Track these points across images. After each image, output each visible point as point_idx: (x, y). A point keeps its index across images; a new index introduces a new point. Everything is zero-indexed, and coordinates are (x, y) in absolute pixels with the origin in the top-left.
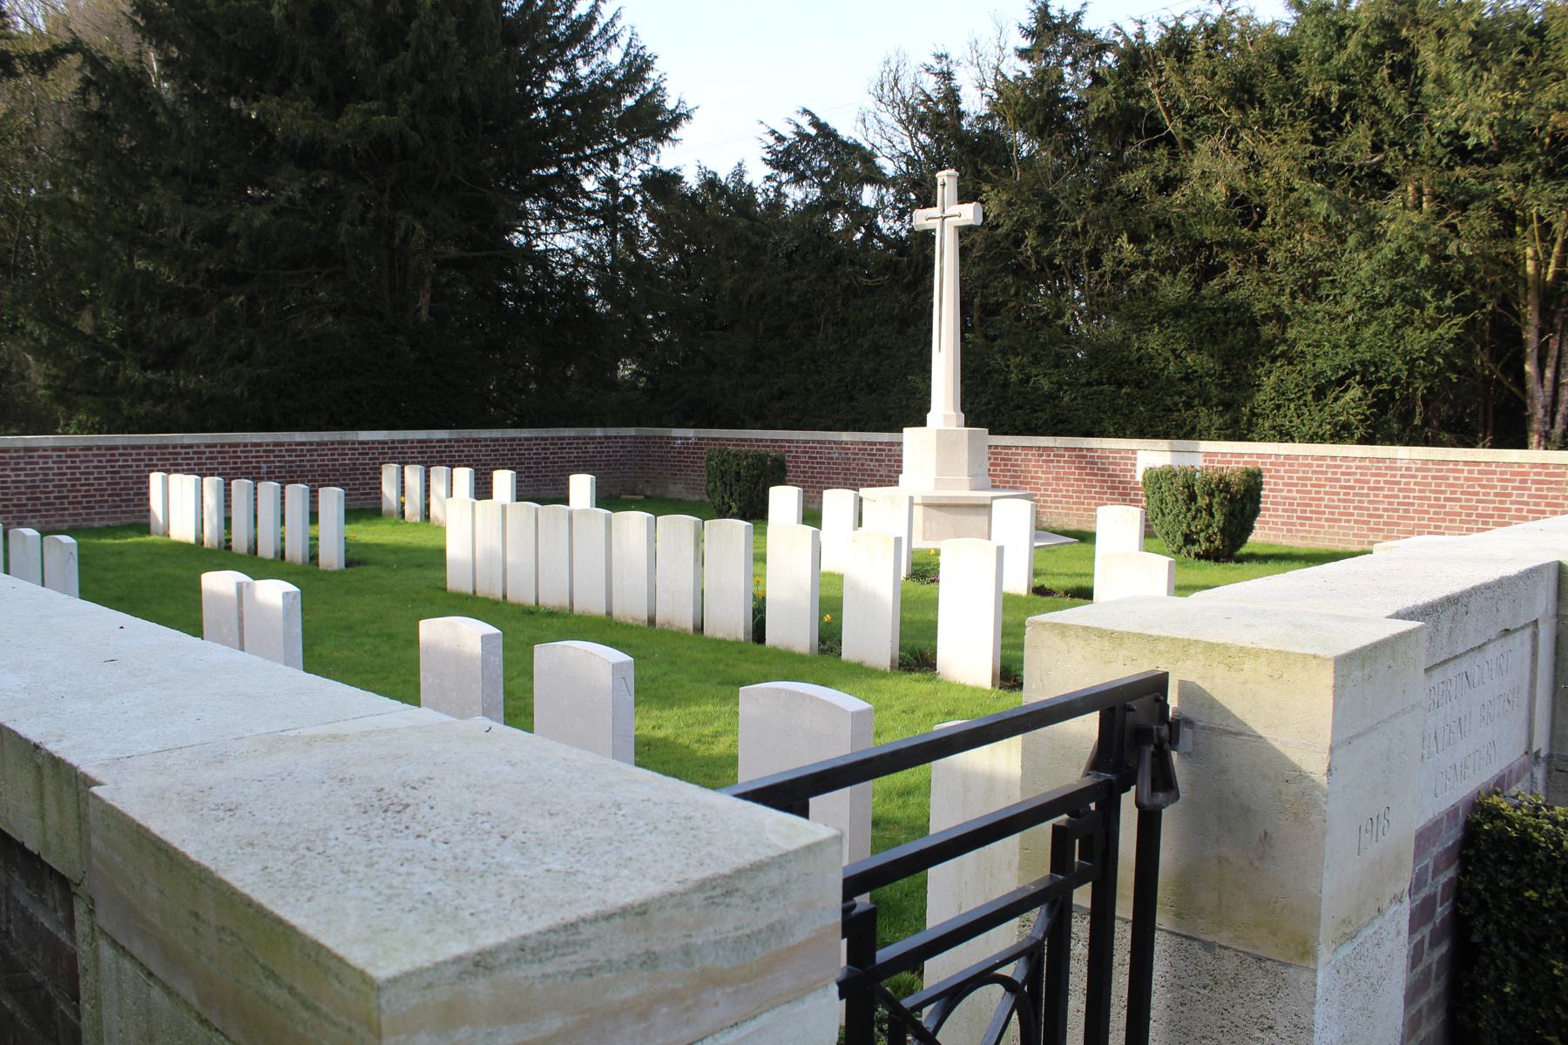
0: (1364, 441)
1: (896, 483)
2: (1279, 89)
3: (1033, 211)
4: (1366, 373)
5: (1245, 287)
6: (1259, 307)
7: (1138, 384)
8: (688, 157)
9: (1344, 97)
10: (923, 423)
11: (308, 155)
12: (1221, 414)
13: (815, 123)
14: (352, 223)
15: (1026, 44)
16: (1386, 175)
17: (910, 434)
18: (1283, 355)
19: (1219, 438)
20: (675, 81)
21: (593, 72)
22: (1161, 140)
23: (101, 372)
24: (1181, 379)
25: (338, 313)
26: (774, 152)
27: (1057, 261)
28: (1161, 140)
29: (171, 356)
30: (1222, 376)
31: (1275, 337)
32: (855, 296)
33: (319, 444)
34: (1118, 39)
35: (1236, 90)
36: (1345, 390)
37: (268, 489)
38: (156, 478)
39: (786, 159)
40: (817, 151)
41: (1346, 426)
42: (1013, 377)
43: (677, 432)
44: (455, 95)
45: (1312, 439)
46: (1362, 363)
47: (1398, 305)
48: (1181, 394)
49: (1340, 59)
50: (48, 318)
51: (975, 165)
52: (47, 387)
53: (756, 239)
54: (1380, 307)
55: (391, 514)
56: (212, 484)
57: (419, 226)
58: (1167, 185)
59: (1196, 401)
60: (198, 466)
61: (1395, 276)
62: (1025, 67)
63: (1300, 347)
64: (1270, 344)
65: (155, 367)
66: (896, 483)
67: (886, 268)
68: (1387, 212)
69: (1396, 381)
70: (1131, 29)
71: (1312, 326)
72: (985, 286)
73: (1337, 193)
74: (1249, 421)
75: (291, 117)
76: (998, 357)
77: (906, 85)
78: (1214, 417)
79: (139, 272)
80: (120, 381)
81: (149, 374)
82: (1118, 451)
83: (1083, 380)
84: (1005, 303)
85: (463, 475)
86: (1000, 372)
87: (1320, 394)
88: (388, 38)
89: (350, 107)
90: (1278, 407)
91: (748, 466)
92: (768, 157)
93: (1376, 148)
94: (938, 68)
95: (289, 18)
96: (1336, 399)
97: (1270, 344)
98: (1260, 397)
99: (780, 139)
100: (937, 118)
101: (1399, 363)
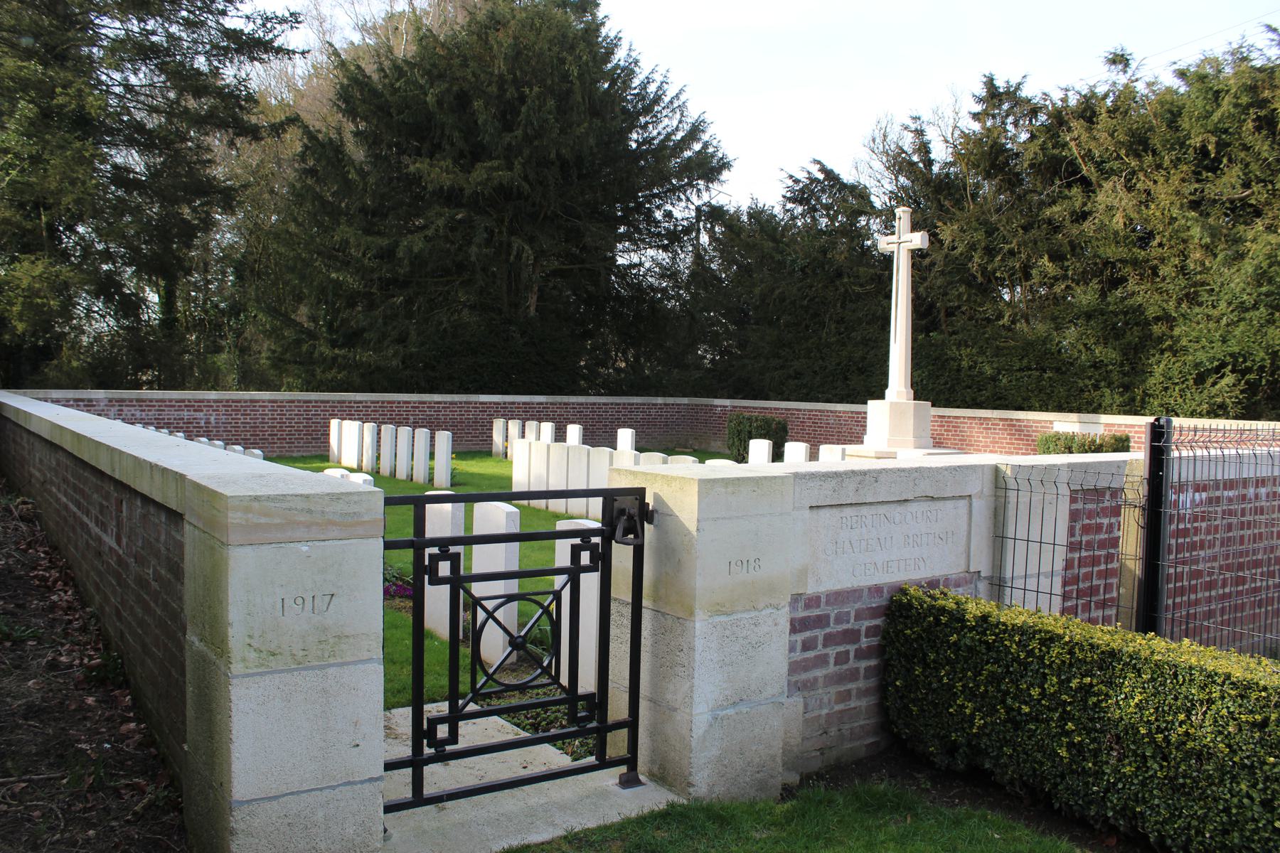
0: (1236, 418)
1: (862, 442)
2: (1168, 141)
3: (979, 236)
4: (1238, 363)
5: (1138, 292)
6: (1151, 312)
7: (1058, 370)
8: (736, 192)
9: (1221, 145)
10: (882, 397)
11: (451, 197)
12: (1122, 394)
13: (823, 169)
14: (479, 246)
15: (978, 108)
16: (1252, 205)
17: (872, 405)
18: (1170, 348)
19: (1119, 413)
20: (724, 136)
21: (659, 134)
22: (1075, 181)
23: (305, 348)
24: (1091, 367)
25: (472, 307)
26: (792, 191)
27: (998, 275)
28: (1075, 181)
29: (353, 338)
30: (1122, 365)
31: (1164, 334)
32: (851, 301)
33: (451, 403)
34: (1048, 103)
35: (1131, 143)
36: (1222, 377)
37: (404, 431)
38: (334, 423)
39: (803, 195)
40: (823, 190)
41: (1222, 406)
42: (964, 364)
43: (718, 402)
44: (553, 156)
45: (1193, 414)
46: (1232, 355)
47: (1262, 309)
48: (1090, 378)
49: (1216, 116)
50: (273, 312)
51: (939, 201)
52: (268, 358)
53: (778, 257)
54: (1247, 310)
55: (498, 455)
56: (369, 427)
57: (527, 247)
58: (1081, 216)
59: (1103, 384)
60: (360, 413)
61: (1260, 285)
62: (976, 127)
63: (1184, 342)
64: (1160, 340)
65: (341, 347)
66: (862, 442)
67: (872, 279)
68: (1250, 235)
69: (1262, 368)
70: (1057, 96)
71: (1194, 325)
72: (945, 294)
73: (1211, 220)
74: (1143, 401)
75: (436, 172)
76: (954, 348)
77: (892, 137)
78: (1116, 397)
79: (332, 281)
80: (316, 355)
81: (337, 351)
82: (1039, 422)
83: (1017, 366)
84: (959, 307)
85: (548, 428)
86: (954, 359)
87: (1200, 380)
88: (507, 115)
89: (479, 165)
90: (1166, 389)
91: (757, 427)
92: (788, 195)
93: (1246, 185)
94: (913, 127)
95: (440, 103)
96: (1214, 384)
97: (1160, 340)
98: (1152, 381)
99: (797, 181)
100: (911, 166)
101: (1262, 354)
